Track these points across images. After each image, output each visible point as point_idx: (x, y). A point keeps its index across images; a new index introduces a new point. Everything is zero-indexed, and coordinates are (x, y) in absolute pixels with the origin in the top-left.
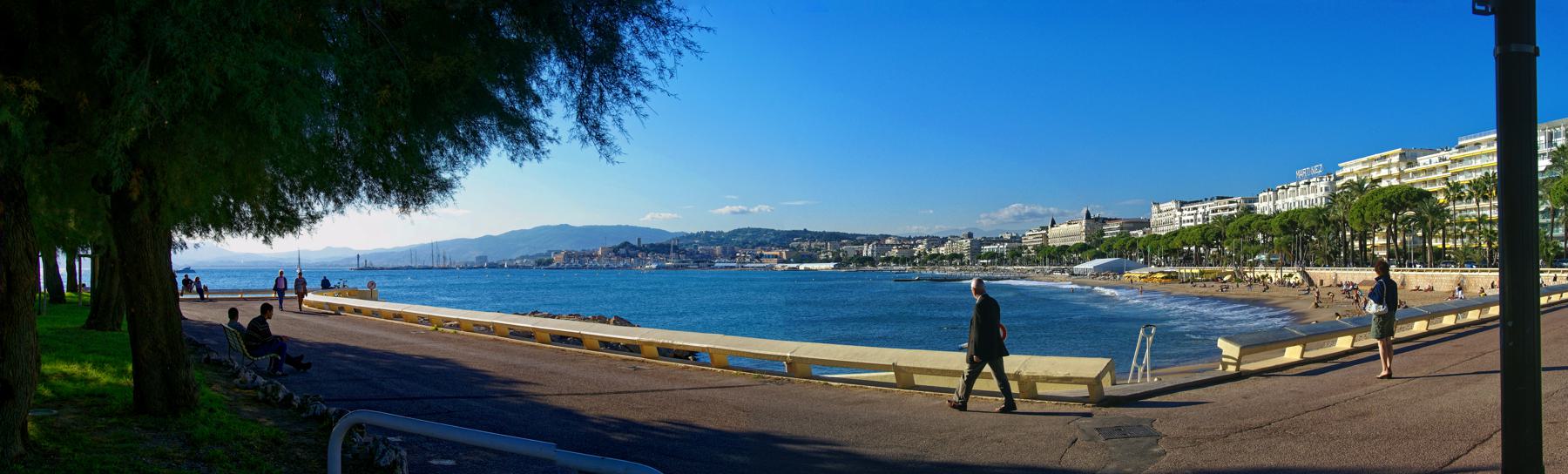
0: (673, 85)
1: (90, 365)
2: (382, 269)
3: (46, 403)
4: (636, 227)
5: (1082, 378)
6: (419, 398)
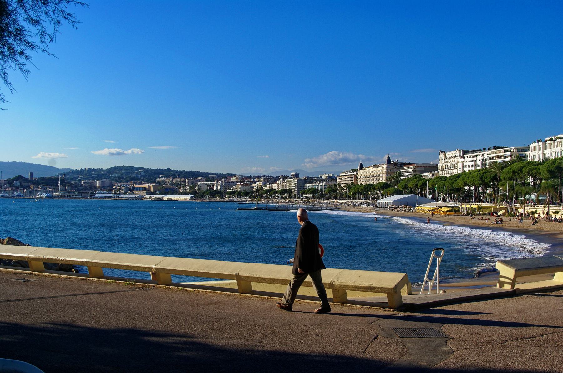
0: (52, 48)
5: (382, 288)
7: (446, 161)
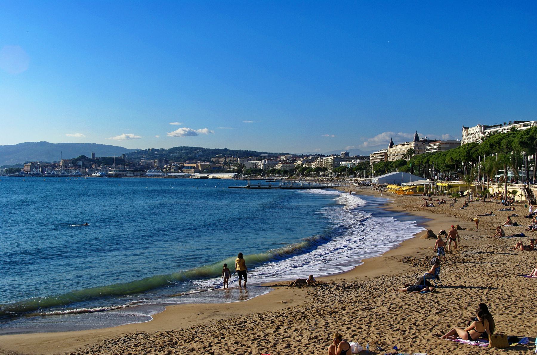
7: (468, 137)
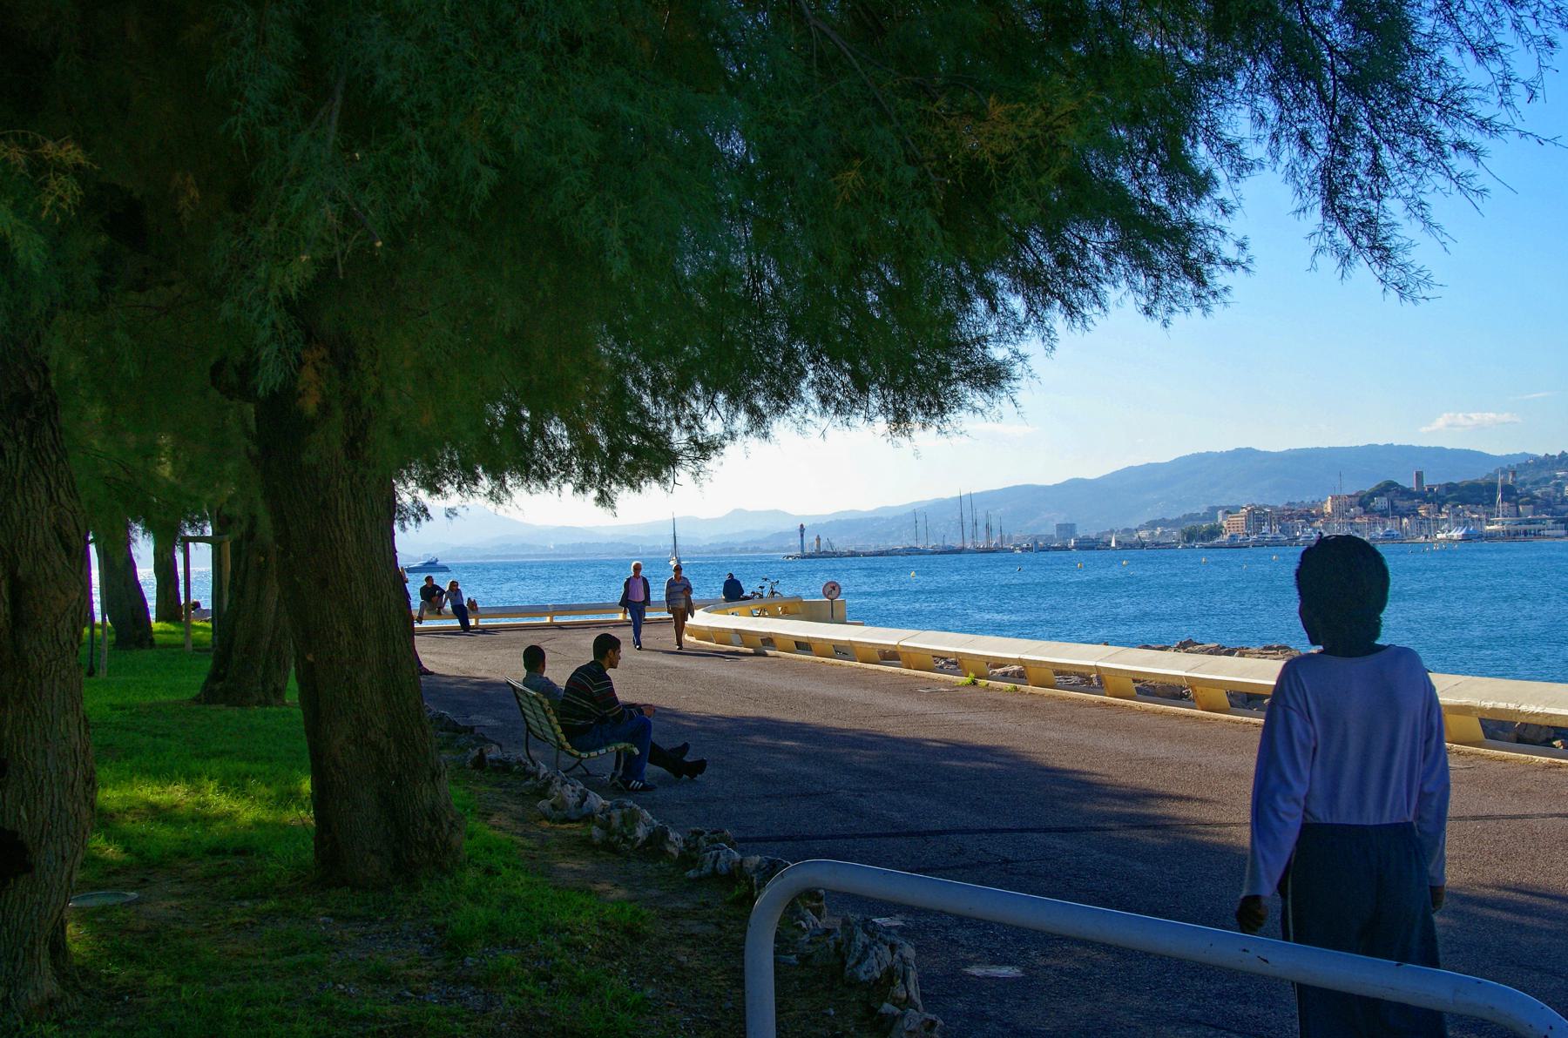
1: (213, 785)
2: (853, 554)
3: (110, 875)
4: (1411, 448)
6: (939, 833)
